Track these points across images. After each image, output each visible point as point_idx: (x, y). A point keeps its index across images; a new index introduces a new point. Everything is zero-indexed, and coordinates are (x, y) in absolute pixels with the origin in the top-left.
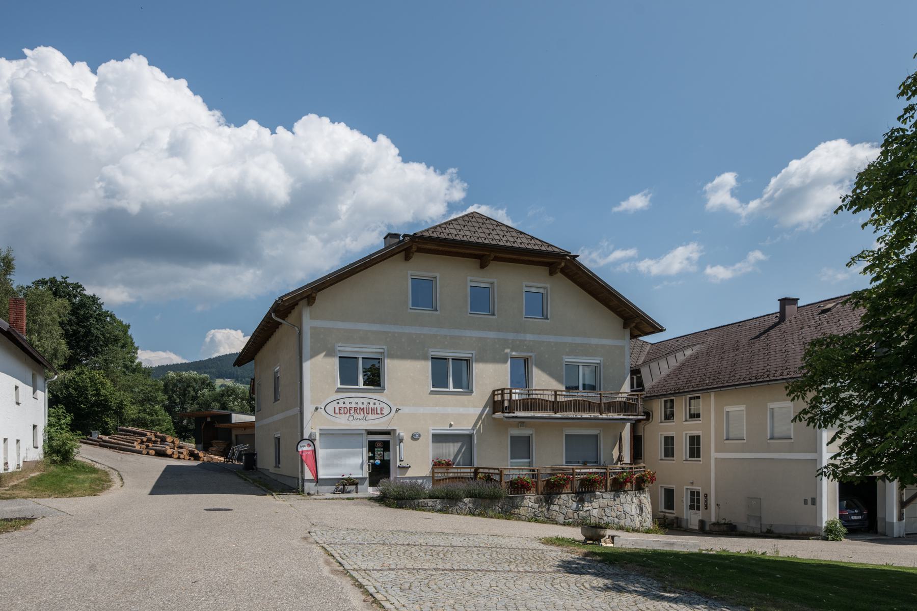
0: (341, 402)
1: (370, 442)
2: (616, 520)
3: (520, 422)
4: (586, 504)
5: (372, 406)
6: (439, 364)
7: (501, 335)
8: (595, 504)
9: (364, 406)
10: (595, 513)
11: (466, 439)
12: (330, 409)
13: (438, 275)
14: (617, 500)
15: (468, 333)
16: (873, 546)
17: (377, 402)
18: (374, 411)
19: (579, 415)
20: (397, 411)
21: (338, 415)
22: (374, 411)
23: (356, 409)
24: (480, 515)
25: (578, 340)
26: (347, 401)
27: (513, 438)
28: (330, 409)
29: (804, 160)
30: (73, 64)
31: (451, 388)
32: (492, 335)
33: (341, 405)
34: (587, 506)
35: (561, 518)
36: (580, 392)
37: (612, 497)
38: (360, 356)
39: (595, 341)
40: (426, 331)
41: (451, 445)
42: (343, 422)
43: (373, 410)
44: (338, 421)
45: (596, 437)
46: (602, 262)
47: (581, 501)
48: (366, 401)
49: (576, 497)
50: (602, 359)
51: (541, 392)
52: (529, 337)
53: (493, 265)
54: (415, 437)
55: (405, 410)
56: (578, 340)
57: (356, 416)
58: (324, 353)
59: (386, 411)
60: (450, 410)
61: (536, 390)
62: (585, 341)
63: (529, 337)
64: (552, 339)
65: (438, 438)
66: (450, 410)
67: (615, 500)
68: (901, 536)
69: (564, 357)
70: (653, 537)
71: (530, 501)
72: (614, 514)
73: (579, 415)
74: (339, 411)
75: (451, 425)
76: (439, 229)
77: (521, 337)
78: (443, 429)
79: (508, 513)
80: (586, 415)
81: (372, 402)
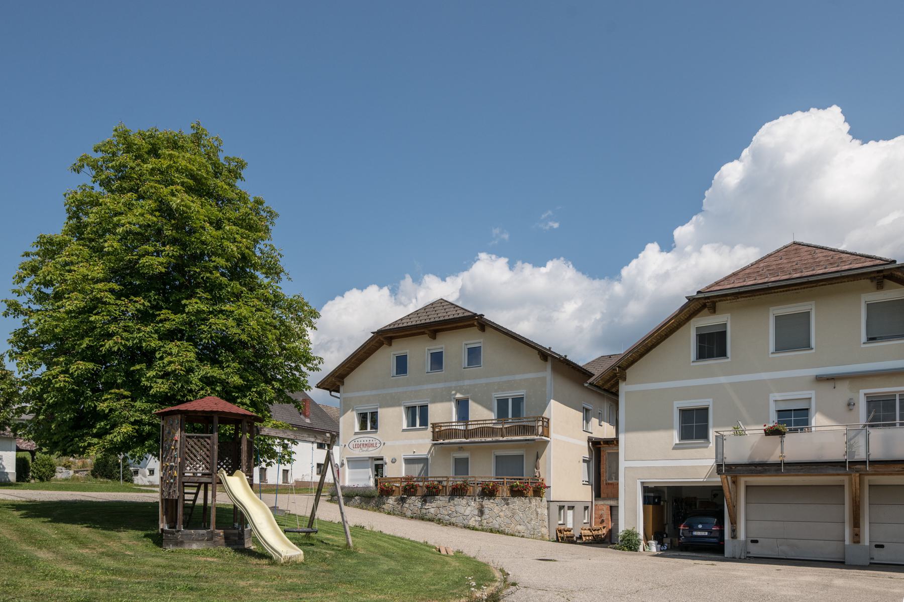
0: (356, 440)
1: (376, 465)
2: (447, 517)
3: (459, 448)
4: (428, 504)
5: (371, 442)
6: (411, 410)
7: (448, 384)
8: (434, 505)
9: (367, 442)
11: (424, 461)
12: (351, 446)
13: (408, 351)
14: (452, 502)
15: (425, 387)
16: (690, 565)
17: (374, 439)
18: (372, 445)
19: (483, 440)
20: (384, 444)
21: (355, 449)
22: (372, 445)
23: (363, 445)
24: (362, 508)
25: (505, 378)
26: (359, 440)
27: (497, 457)
28: (351, 446)
29: (750, 146)
30: (343, 297)
31: (418, 426)
32: (441, 385)
33: (356, 443)
34: (428, 506)
35: (409, 513)
37: (448, 500)
39: (518, 377)
40: (400, 390)
41: (416, 465)
42: (358, 453)
43: (372, 445)
46: (692, 325)
47: (425, 501)
48: (368, 439)
49: (421, 499)
50: (525, 391)
52: (467, 382)
53: (440, 336)
54: (394, 461)
55: (388, 443)
56: (505, 378)
57: (364, 449)
59: (378, 445)
60: (413, 442)
61: (471, 421)
62: (511, 378)
63: (467, 382)
64: (483, 381)
65: (408, 461)
66: (413, 442)
67: (449, 502)
68: (737, 556)
69: (493, 394)
70: (745, 567)
71: (391, 501)
72: (446, 513)
75: (414, 452)
76: (399, 322)
77: (461, 383)
78: (410, 455)
79: (378, 508)
81: (371, 439)
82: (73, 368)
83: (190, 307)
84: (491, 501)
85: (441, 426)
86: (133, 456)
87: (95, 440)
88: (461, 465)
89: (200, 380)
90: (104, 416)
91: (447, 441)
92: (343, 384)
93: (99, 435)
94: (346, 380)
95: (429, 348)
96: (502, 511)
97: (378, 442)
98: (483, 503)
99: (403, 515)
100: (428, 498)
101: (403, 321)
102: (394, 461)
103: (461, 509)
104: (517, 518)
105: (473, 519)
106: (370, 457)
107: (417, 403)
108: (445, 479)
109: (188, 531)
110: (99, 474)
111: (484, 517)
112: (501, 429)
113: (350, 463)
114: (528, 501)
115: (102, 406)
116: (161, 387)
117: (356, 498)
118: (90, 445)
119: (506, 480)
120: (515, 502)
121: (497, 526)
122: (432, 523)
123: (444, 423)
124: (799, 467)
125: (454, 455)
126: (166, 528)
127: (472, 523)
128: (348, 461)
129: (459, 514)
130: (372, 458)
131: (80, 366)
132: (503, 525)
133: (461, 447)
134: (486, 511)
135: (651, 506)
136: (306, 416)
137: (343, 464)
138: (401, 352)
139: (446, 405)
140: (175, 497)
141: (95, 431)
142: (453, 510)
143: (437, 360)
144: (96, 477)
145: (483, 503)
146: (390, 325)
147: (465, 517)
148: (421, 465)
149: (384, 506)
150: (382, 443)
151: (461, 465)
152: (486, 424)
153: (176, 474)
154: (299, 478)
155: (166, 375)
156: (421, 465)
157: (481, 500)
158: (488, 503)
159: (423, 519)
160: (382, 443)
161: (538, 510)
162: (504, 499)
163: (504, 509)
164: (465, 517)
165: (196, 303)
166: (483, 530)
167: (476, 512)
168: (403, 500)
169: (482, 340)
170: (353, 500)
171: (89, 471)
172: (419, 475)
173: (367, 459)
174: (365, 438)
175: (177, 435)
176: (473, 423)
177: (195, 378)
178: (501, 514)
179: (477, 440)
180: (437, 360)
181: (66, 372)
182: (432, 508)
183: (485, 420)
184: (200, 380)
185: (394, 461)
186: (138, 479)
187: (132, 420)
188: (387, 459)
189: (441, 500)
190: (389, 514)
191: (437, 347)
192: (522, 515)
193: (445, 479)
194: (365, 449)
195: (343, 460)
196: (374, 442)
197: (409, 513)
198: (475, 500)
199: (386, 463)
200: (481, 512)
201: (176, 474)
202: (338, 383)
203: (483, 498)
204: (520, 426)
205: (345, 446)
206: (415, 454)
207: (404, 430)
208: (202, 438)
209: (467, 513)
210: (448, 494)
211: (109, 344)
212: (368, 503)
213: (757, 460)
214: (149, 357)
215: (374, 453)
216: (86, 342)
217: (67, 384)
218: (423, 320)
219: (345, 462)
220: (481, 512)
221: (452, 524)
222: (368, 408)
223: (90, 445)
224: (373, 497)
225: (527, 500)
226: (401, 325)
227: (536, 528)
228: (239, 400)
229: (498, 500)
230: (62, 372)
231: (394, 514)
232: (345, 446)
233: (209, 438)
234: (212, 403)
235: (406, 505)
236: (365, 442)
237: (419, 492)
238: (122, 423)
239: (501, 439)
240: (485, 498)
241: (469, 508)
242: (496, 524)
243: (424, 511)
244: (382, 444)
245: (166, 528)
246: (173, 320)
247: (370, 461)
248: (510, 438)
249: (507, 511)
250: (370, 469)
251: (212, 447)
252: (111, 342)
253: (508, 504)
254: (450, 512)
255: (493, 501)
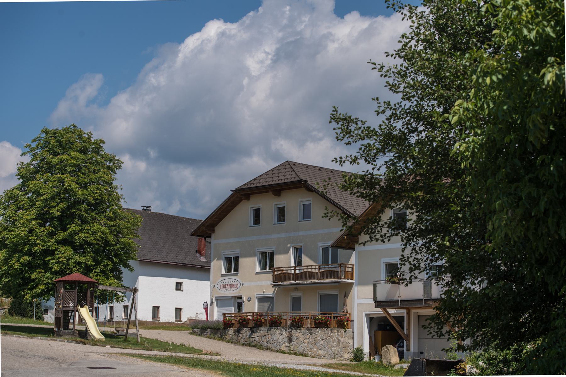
0: (223, 281)
2: (266, 344)
4: (254, 334)
5: (233, 283)
8: (258, 334)
9: (230, 283)
10: (257, 339)
13: (261, 205)
19: (305, 282)
20: (243, 285)
21: (221, 289)
26: (225, 281)
27: (322, 297)
31: (268, 270)
33: (223, 284)
34: (254, 335)
35: (242, 341)
36: (330, 265)
37: (267, 330)
38: (232, 256)
41: (266, 304)
42: (224, 293)
44: (221, 292)
45: (336, 295)
47: (253, 332)
48: (231, 280)
51: (310, 267)
52: (301, 233)
53: (283, 194)
58: (216, 259)
63: (301, 233)
69: (318, 243)
73: (305, 282)
74: (224, 287)
75: (264, 292)
78: (260, 294)
79: (222, 338)
80: (309, 282)
81: (233, 280)
82: (22, 260)
83: (71, 229)
84: (298, 331)
85: (282, 270)
86: (44, 299)
87: (29, 292)
88: (297, 303)
89: (74, 263)
90: (33, 280)
91: (285, 283)
92: (214, 232)
93: (31, 289)
94: (216, 228)
95: (276, 203)
96: (306, 338)
97: (238, 282)
98: (292, 333)
99: (238, 343)
100: (255, 329)
101: (256, 181)
102: (249, 299)
103: (275, 337)
104: (319, 344)
105: (284, 345)
106: (233, 296)
107: (268, 249)
108: (285, 314)
109: (64, 331)
110: (14, 312)
111: (292, 343)
112: (317, 273)
113: (219, 302)
114: (329, 331)
115: (33, 276)
116: (56, 268)
117: (209, 330)
118: (27, 293)
119: (332, 315)
120: (318, 332)
121: (302, 351)
122: (255, 348)
123: (285, 267)
124: (407, 303)
125: (292, 294)
126: (56, 330)
127: (283, 348)
128: (217, 300)
129: (274, 341)
130: (235, 297)
131: (25, 259)
132: (306, 350)
133: (296, 288)
134: (294, 339)
135: (381, 332)
136: (201, 255)
137: (212, 303)
138: (256, 206)
139: (250, 259)
140: (60, 316)
141: (29, 287)
142: (270, 338)
143: (281, 212)
144: (12, 315)
145: (292, 333)
146: (245, 185)
147: (278, 344)
148: (269, 303)
149: (225, 336)
150: (241, 284)
151: (297, 303)
152: (311, 269)
153: (61, 307)
154: (193, 316)
155: (59, 262)
156: (269, 303)
157: (290, 330)
158: (296, 333)
159: (250, 346)
160: (241, 284)
161: (340, 339)
162: (309, 330)
163: (308, 337)
164: (278, 344)
165: (74, 227)
166: (290, 353)
167: (286, 340)
168: (238, 331)
169: (311, 199)
170: (206, 332)
171: (7, 310)
172: (268, 310)
173: (231, 298)
174: (229, 280)
175: (62, 291)
176: (315, 267)
177: (71, 262)
178: (305, 341)
179: (302, 282)
180: (281, 212)
181: (18, 261)
182: (257, 337)
183: (307, 266)
184: (74, 263)
185: (249, 300)
186: (47, 318)
187: (45, 282)
188: (245, 299)
189: (263, 331)
190: (228, 342)
191: (282, 202)
192: (323, 342)
193: (285, 314)
194: (229, 289)
195: (212, 299)
196: (236, 283)
197: (242, 341)
198: (286, 330)
199: (244, 302)
200: (290, 340)
201: (61, 307)
202: (209, 232)
203: (292, 329)
204: (329, 271)
205: (214, 286)
206: (265, 293)
207: (257, 273)
208: (71, 291)
209: (280, 340)
210: (268, 325)
211: (36, 248)
212: (215, 334)
213: (389, 299)
214: (51, 253)
215: (234, 292)
216: (26, 248)
217: (18, 267)
218: (263, 183)
219: (214, 301)
220: (290, 340)
221: (268, 349)
222: (232, 253)
223: (27, 293)
224: (219, 329)
225: (329, 331)
226: (252, 186)
227: (336, 352)
228: (94, 271)
229: (303, 330)
230: (17, 261)
231: (232, 342)
232: (214, 286)
233: (74, 291)
234: (77, 276)
235: (241, 335)
236: (229, 283)
237: (250, 326)
238: (41, 285)
239: (317, 281)
240: (294, 329)
241: (281, 337)
242: (300, 349)
243: (251, 339)
244: (241, 285)
245: (56, 330)
246: (61, 235)
247: (233, 300)
248: (322, 281)
249: (310, 339)
250: (233, 307)
251: (75, 295)
252: (37, 248)
253: (311, 333)
254: (268, 340)
255: (299, 331)
